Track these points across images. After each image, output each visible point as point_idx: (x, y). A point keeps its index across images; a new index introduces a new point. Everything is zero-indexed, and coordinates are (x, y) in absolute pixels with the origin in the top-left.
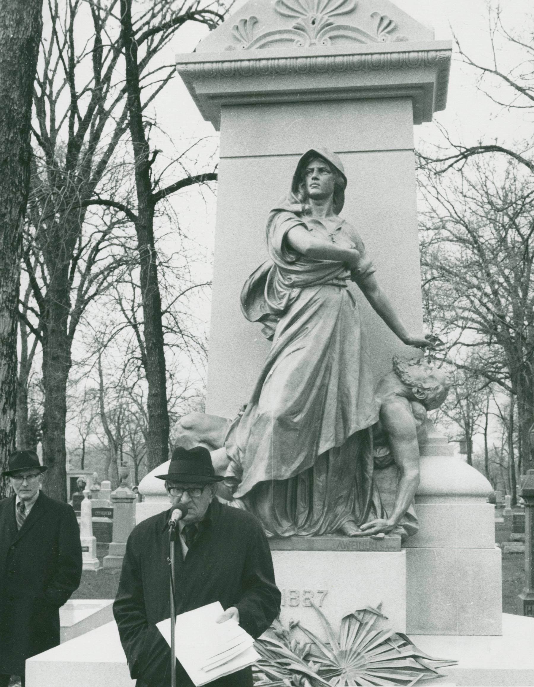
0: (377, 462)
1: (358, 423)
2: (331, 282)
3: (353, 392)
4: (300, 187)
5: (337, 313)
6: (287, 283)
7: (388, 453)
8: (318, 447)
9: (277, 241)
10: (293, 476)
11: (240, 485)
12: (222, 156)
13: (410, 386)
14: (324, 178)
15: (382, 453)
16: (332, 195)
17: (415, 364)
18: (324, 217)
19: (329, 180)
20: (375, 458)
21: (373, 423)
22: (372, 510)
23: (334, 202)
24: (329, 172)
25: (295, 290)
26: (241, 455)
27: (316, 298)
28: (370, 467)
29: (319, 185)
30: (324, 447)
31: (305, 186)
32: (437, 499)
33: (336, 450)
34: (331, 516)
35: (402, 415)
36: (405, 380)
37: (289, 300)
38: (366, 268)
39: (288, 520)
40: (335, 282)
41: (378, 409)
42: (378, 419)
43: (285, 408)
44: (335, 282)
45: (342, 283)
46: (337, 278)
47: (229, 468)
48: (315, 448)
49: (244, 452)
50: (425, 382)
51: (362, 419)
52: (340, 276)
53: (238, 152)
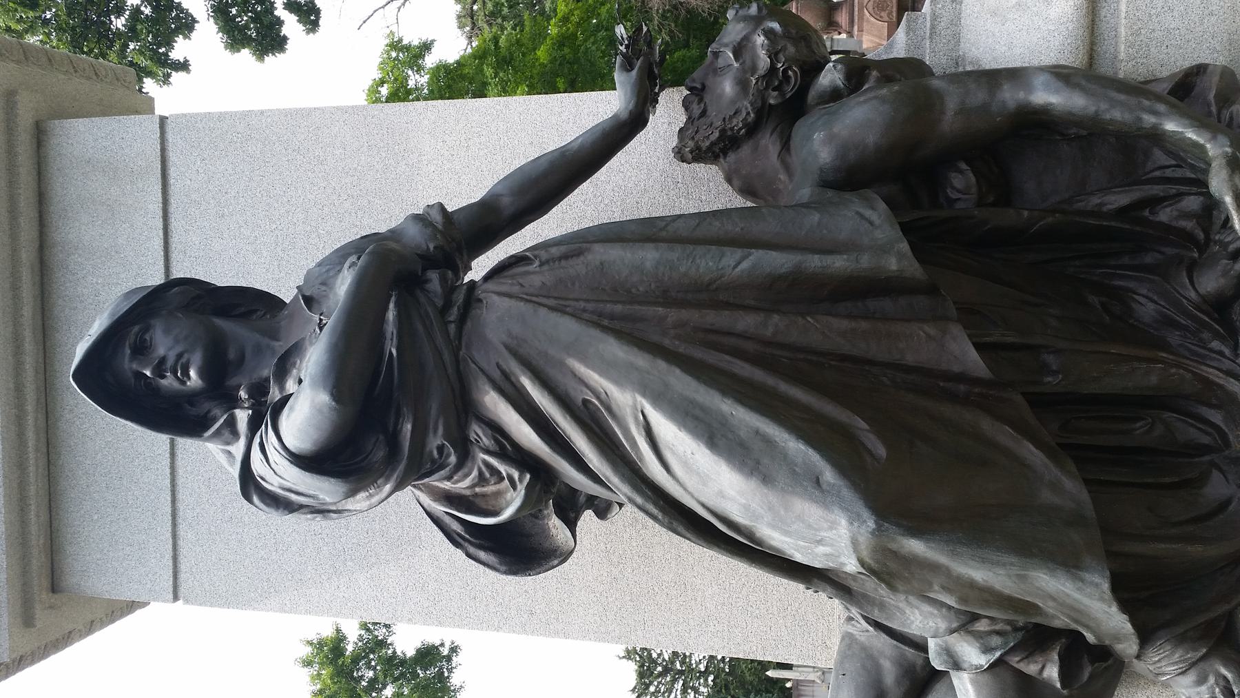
0: (991, 199)
1: (884, 249)
2: (452, 328)
3: (779, 261)
4: (194, 411)
5: (543, 311)
6: (453, 459)
7: (963, 166)
8: (961, 378)
9: (322, 489)
10: (1073, 468)
11: (1090, 638)
12: (171, 596)
13: (763, 114)
14: (163, 344)
15: (961, 181)
16: (219, 322)
17: (701, 100)
18: (277, 344)
19: (167, 331)
20: (980, 204)
21: (882, 206)
22: (1146, 213)
23: (245, 316)
24: (147, 329)
25: (473, 436)
26: (982, 626)
27: (497, 375)
28: (1007, 217)
29: (180, 356)
30: (963, 353)
31: (192, 397)
32: (1103, 27)
33: (971, 316)
34: (1174, 338)
35: (861, 120)
36: (746, 125)
37: (502, 455)
38: (429, 231)
39: (1203, 479)
40: (454, 314)
41: (830, 193)
42: (869, 193)
43: (847, 493)
44: (454, 314)
45: (460, 297)
46: (444, 310)
47: (1031, 669)
48: (962, 388)
49: (975, 617)
50: (754, 69)
51: (871, 237)
52: (440, 303)
53: (162, 557)
